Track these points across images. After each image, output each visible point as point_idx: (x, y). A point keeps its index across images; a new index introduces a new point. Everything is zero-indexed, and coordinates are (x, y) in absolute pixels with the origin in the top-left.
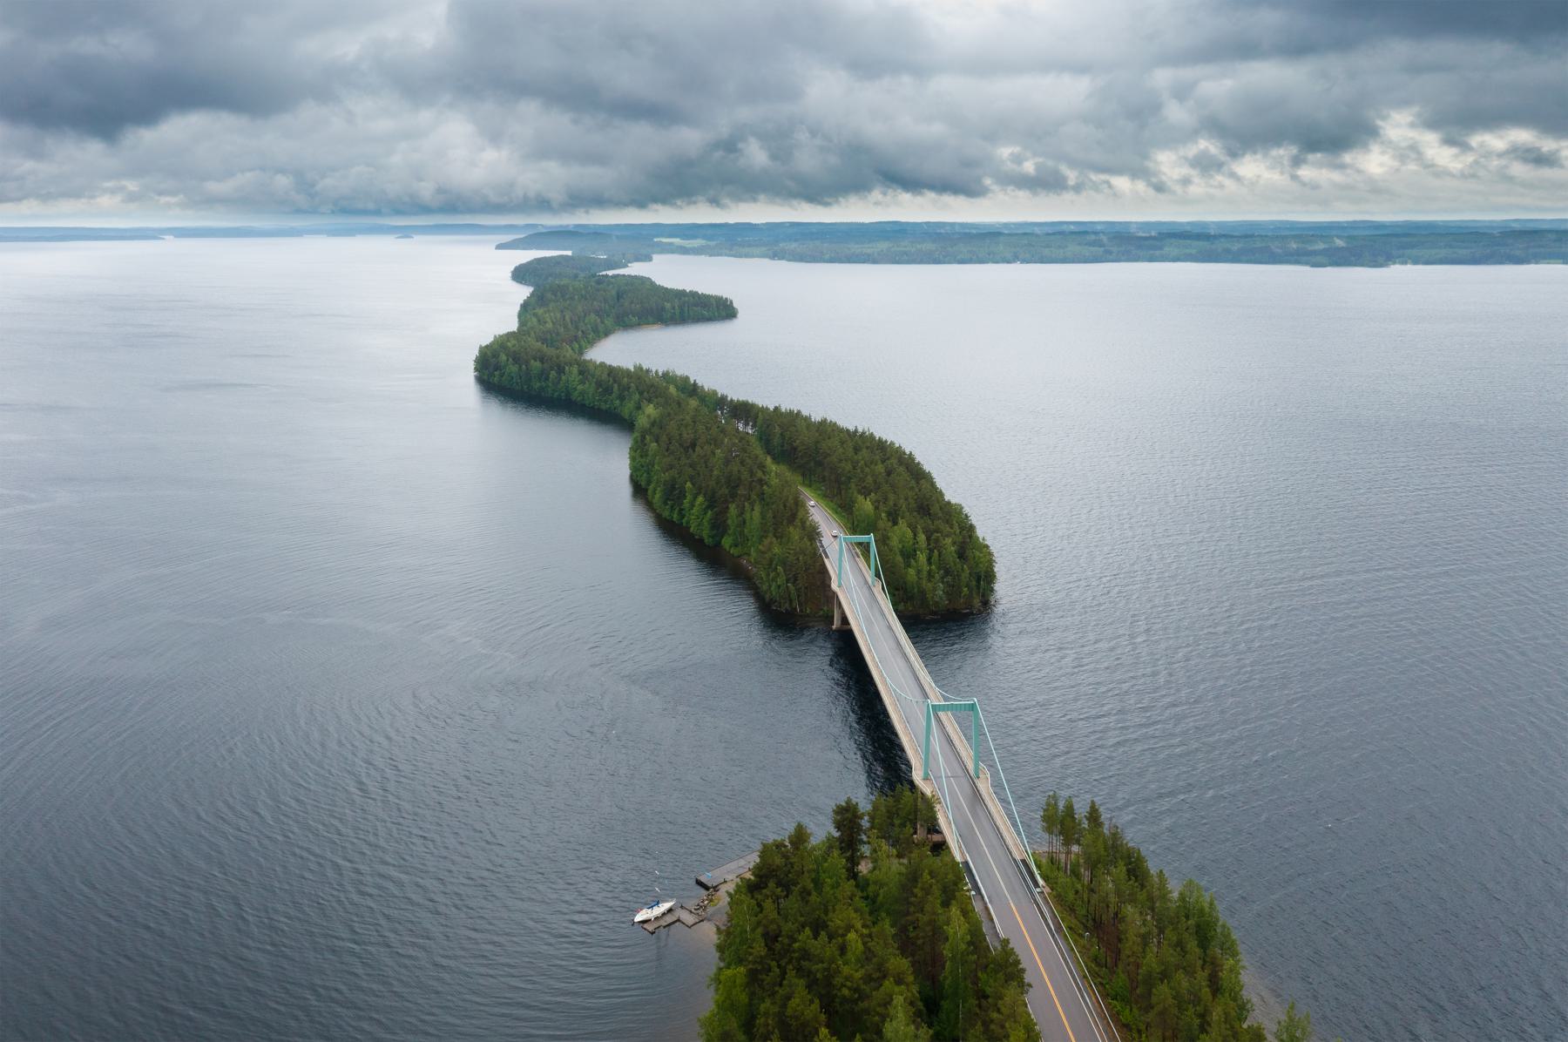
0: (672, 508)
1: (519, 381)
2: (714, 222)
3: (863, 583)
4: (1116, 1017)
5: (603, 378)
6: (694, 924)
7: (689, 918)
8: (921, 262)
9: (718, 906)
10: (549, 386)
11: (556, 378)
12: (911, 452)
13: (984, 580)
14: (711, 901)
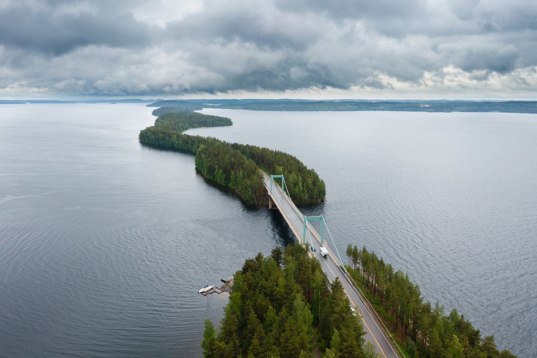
0: (211, 176)
1: (155, 141)
3: (279, 192)
4: (376, 309)
5: (185, 139)
10: (166, 142)
12: (295, 157)
13: (322, 193)
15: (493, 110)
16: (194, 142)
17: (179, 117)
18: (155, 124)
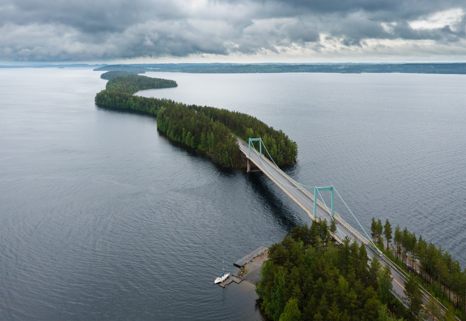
0: (178, 137)
1: (112, 103)
2: (162, 63)
6: (240, 282)
7: (238, 280)
8: (229, 73)
9: (247, 274)
11: (125, 102)
12: (255, 117)
14: (244, 272)
15: (395, 71)
16: (152, 104)
17: (129, 81)
18: (107, 87)
